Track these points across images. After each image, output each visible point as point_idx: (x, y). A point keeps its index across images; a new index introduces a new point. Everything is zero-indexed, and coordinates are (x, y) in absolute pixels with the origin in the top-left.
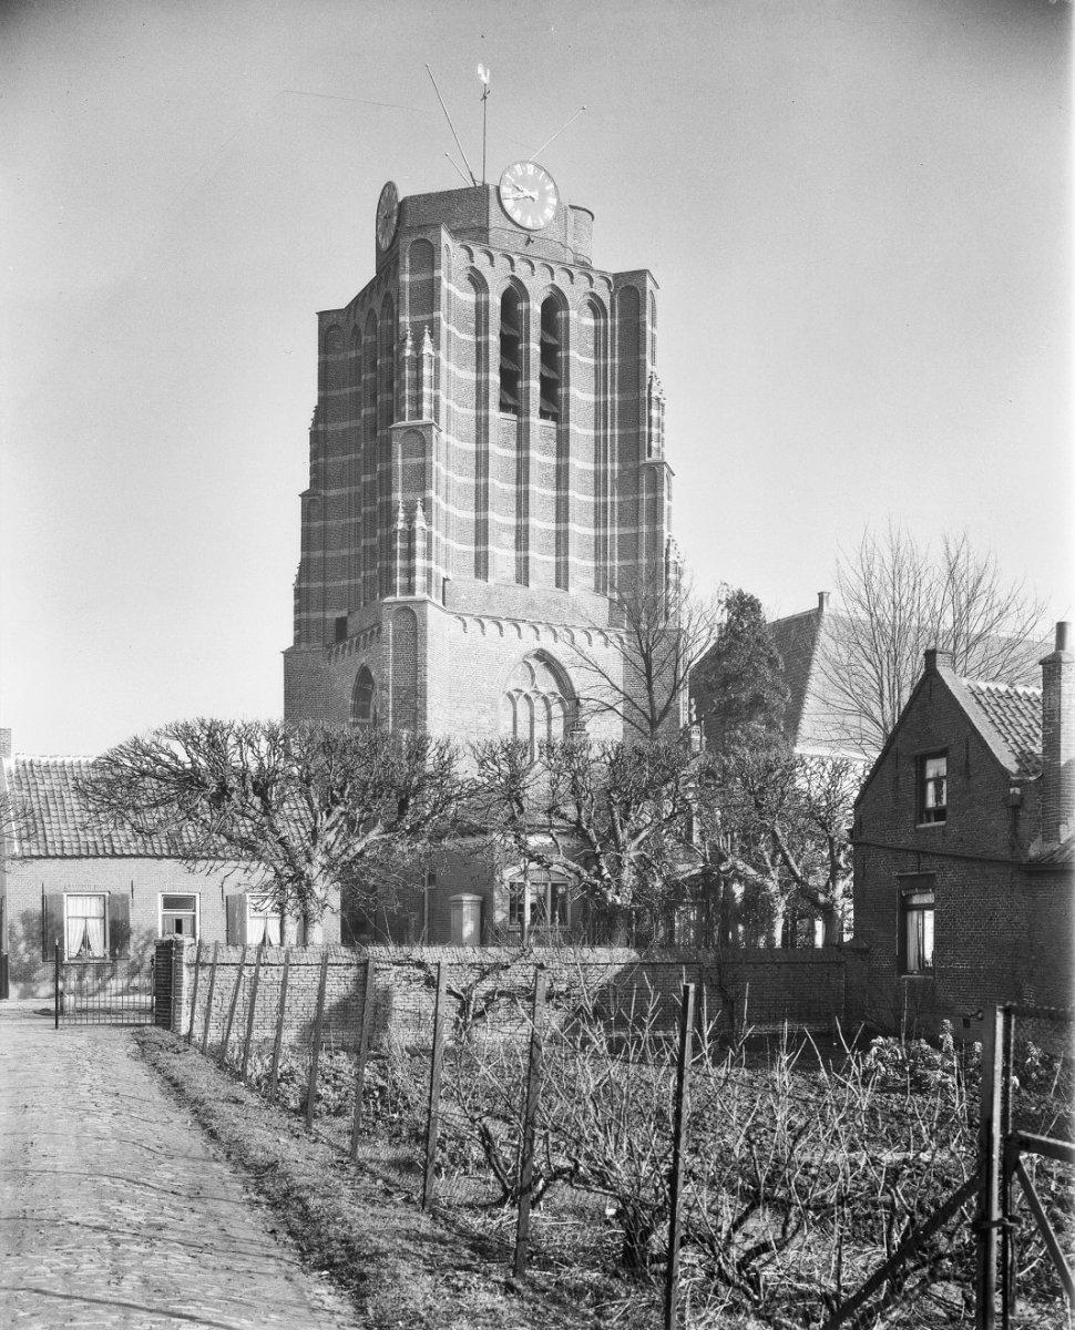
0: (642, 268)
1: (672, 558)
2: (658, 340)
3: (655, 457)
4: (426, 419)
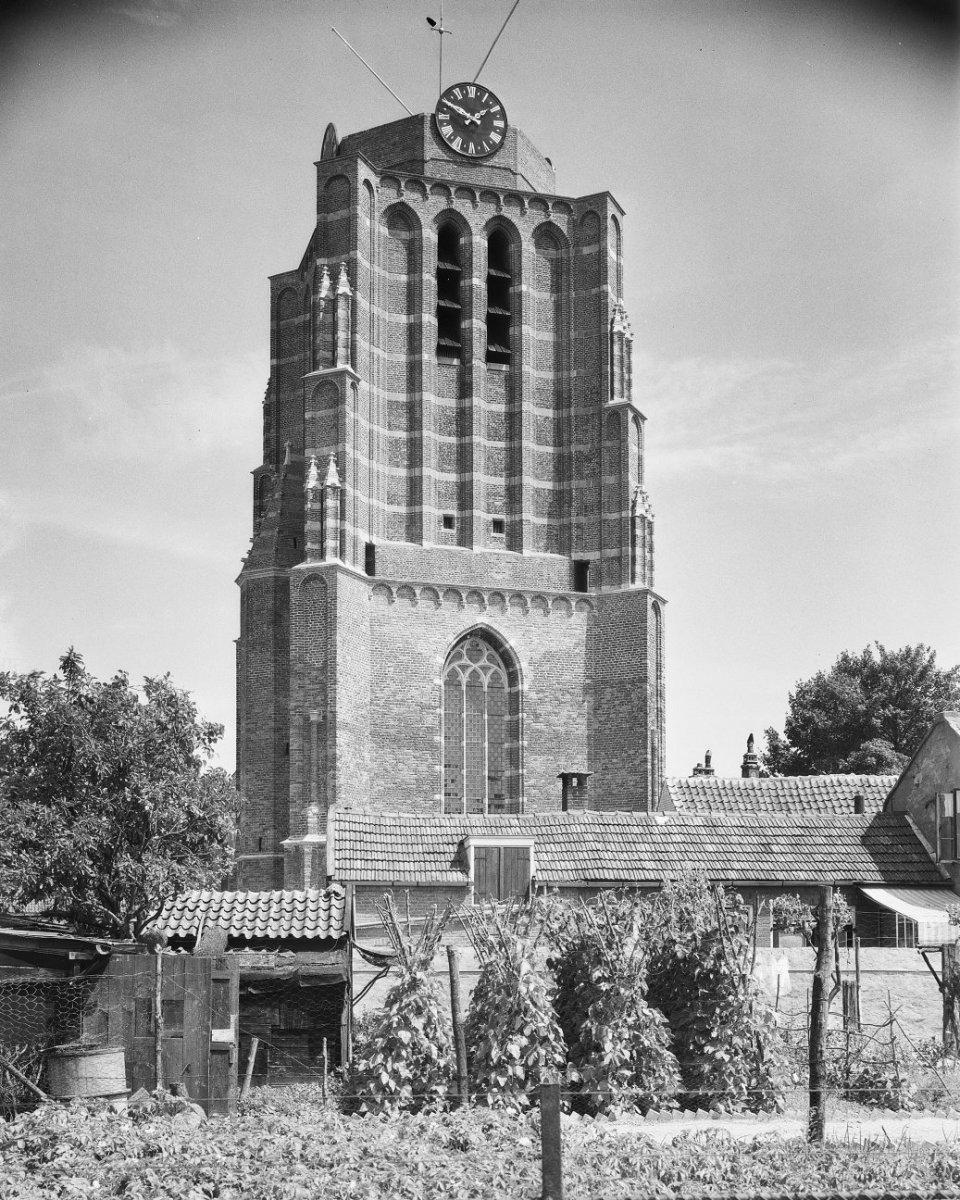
0: (601, 191)
1: (639, 511)
2: (625, 275)
3: (617, 400)
4: (341, 366)
